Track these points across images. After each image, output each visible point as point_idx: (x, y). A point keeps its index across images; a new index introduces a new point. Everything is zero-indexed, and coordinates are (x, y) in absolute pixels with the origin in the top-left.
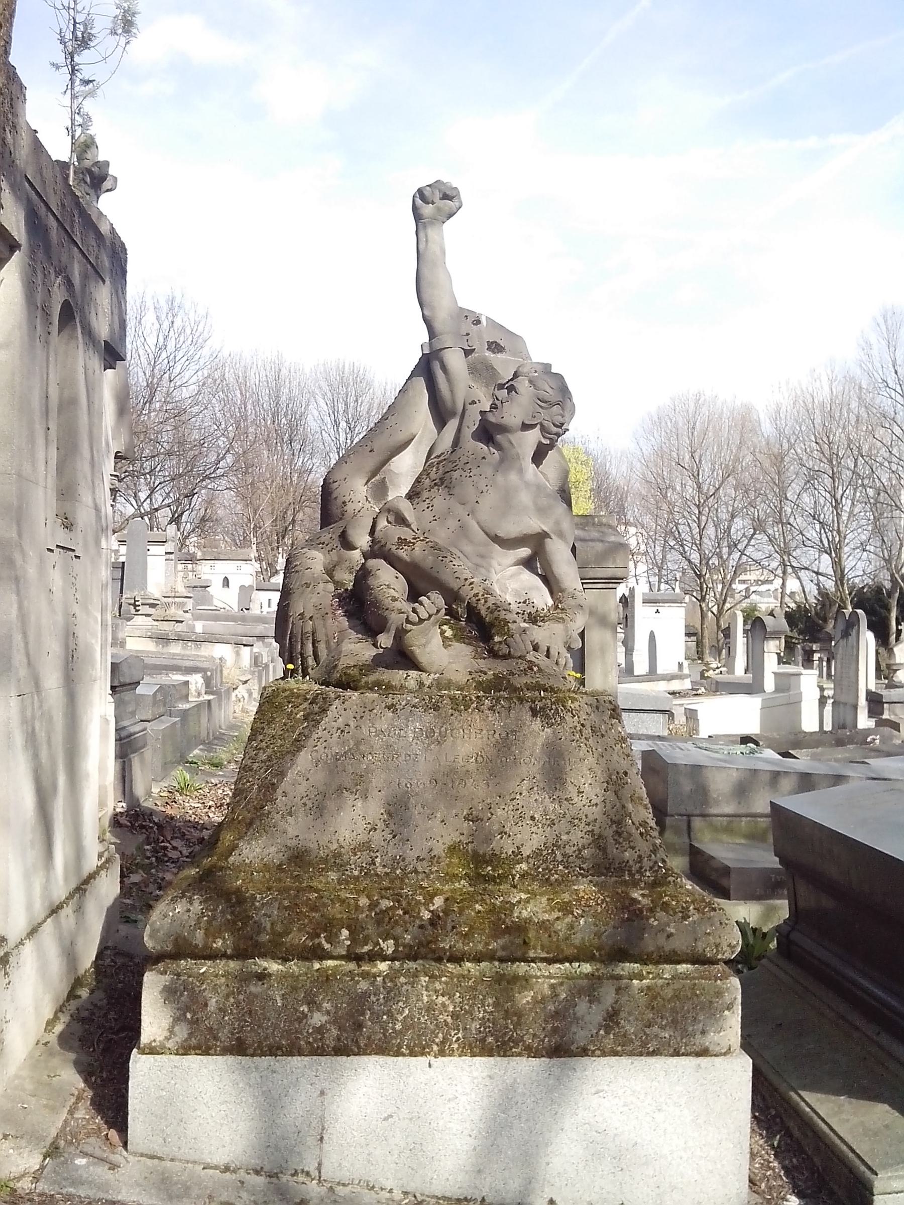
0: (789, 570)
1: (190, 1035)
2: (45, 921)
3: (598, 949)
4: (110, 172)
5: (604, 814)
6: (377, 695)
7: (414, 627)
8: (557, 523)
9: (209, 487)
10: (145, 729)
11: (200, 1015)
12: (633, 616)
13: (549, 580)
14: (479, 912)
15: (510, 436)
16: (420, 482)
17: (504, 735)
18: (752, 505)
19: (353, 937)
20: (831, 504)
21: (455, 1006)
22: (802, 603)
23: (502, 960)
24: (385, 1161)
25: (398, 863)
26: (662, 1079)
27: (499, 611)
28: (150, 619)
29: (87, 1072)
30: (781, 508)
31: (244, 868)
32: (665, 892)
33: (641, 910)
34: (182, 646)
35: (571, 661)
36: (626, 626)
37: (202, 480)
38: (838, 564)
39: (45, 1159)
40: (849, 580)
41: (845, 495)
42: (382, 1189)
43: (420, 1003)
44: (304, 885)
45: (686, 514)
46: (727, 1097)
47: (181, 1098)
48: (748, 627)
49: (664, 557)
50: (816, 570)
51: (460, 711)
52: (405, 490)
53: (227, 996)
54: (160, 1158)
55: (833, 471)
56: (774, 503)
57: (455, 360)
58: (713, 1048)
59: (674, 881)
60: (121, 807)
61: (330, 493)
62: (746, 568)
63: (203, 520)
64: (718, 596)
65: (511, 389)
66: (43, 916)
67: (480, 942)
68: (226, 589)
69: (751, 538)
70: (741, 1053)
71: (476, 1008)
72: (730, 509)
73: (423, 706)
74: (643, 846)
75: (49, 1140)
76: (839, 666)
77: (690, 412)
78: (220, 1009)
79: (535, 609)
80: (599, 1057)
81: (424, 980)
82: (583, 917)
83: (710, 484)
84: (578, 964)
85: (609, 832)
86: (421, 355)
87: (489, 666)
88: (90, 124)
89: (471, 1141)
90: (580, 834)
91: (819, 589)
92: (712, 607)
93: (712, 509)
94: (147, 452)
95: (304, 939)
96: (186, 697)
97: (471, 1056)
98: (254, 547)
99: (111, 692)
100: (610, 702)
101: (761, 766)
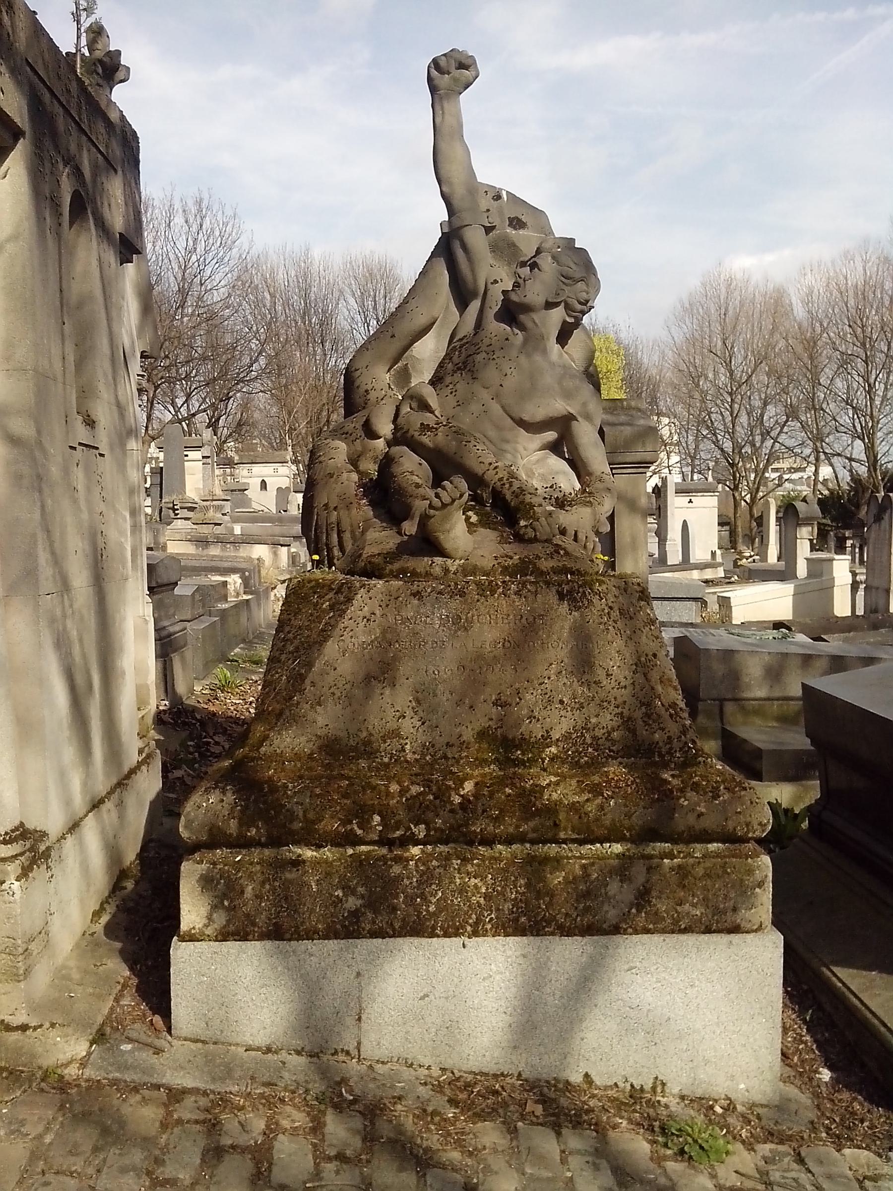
0: (822, 456)
1: (228, 922)
2: (86, 816)
3: (629, 830)
4: (122, 63)
5: (633, 696)
6: (401, 583)
7: (437, 513)
8: (584, 404)
9: (244, 390)
10: (185, 629)
11: (236, 903)
12: (666, 506)
13: (577, 465)
14: (509, 795)
15: (535, 316)
16: (443, 367)
17: (531, 619)
18: (785, 391)
19: (384, 822)
20: (865, 389)
21: (487, 888)
22: (834, 490)
23: (533, 842)
24: (423, 1039)
25: (428, 750)
26: (694, 956)
27: (524, 495)
28: (189, 522)
29: (131, 959)
30: (814, 394)
31: (278, 758)
32: (695, 772)
33: (671, 791)
34: (222, 548)
35: (599, 545)
36: (660, 517)
37: (237, 384)
38: (870, 449)
39: (91, 1046)
40: (882, 465)
41: (878, 379)
42: (420, 1066)
43: (453, 885)
44: (335, 773)
45: (719, 402)
46: (759, 973)
47: (221, 982)
48: (781, 515)
49: (697, 447)
50: (849, 456)
51: (486, 597)
52: (428, 376)
53: (263, 883)
54: (203, 1042)
55: (866, 354)
56: (806, 389)
57: (476, 238)
58: (745, 925)
59: (704, 761)
60: (165, 704)
61: (353, 382)
62: (779, 456)
63: (240, 424)
64: (751, 485)
65: (534, 266)
66: (84, 811)
67: (511, 825)
68: (264, 492)
69: (784, 425)
70: (771, 930)
71: (508, 890)
72: (763, 396)
73: (448, 593)
74: (673, 728)
75: (96, 1027)
76: (871, 554)
77: (722, 298)
78: (257, 896)
79: (562, 494)
80: (631, 934)
81: (456, 863)
82: (612, 798)
83: (743, 372)
84: (608, 845)
85: (639, 714)
86: (440, 235)
87: (515, 551)
88: (95, 7)
89: (507, 1018)
90: (609, 717)
91: (852, 475)
92: (746, 496)
93: (745, 397)
94: (182, 358)
95: (336, 825)
96: (225, 598)
97: (504, 936)
98: (290, 448)
99: (148, 593)
100: (639, 584)
101: (793, 649)
